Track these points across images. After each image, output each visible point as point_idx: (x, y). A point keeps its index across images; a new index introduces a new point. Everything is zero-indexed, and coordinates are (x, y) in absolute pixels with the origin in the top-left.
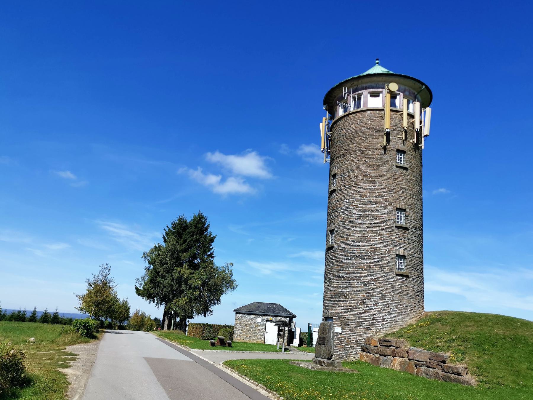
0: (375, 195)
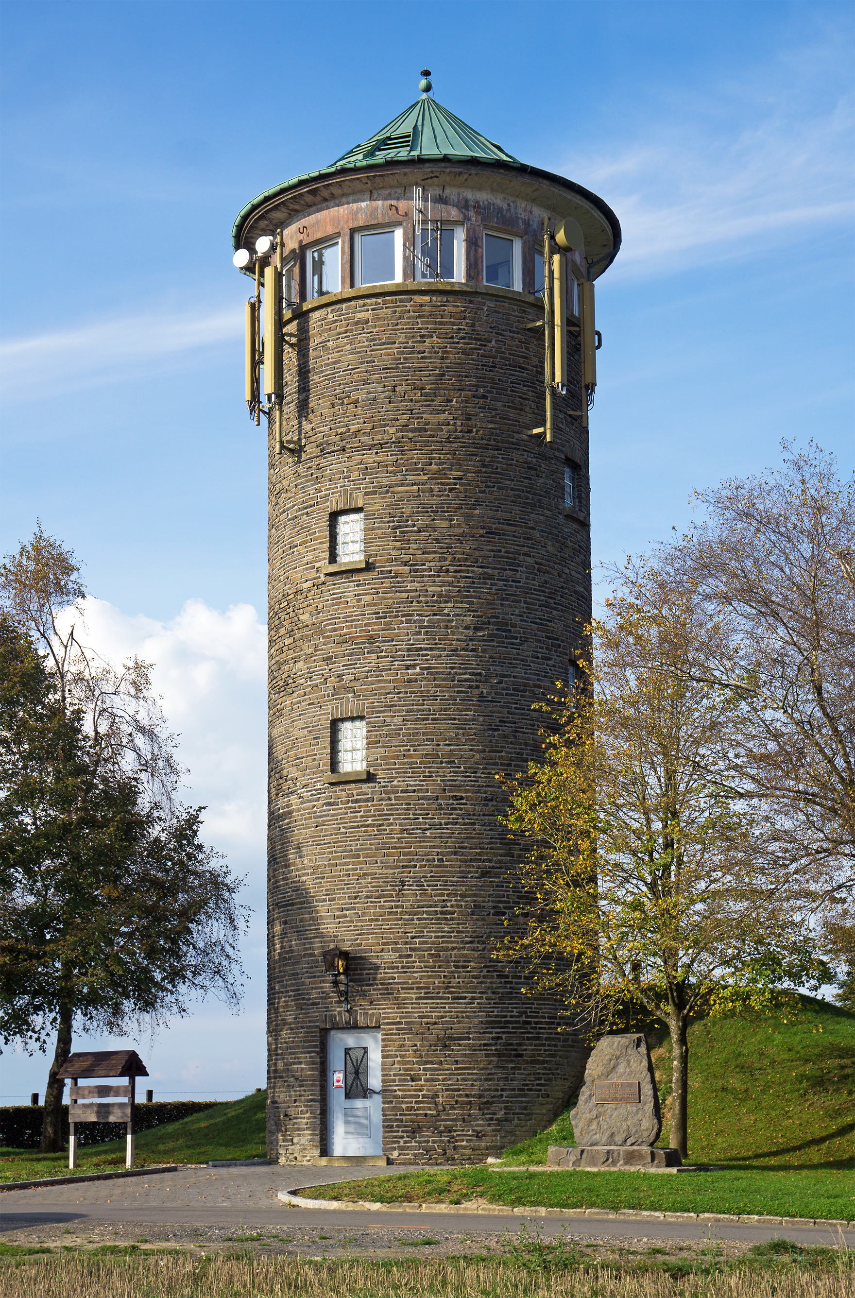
0: (517, 612)
